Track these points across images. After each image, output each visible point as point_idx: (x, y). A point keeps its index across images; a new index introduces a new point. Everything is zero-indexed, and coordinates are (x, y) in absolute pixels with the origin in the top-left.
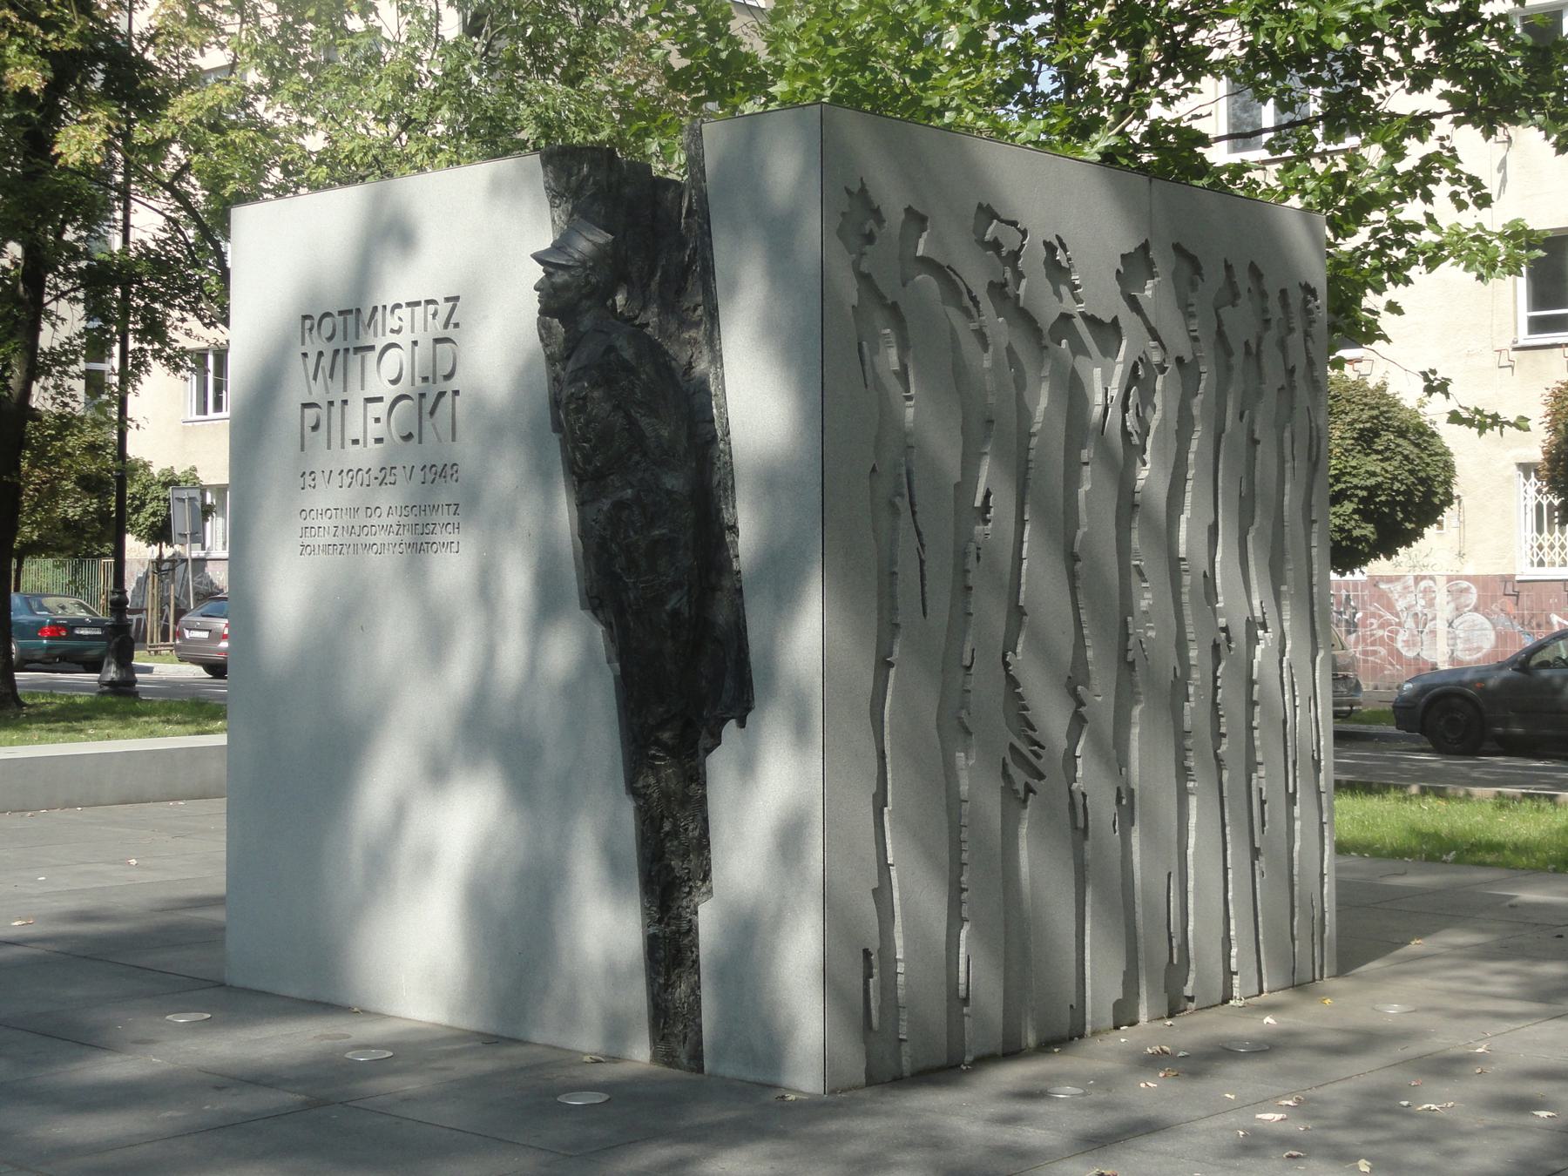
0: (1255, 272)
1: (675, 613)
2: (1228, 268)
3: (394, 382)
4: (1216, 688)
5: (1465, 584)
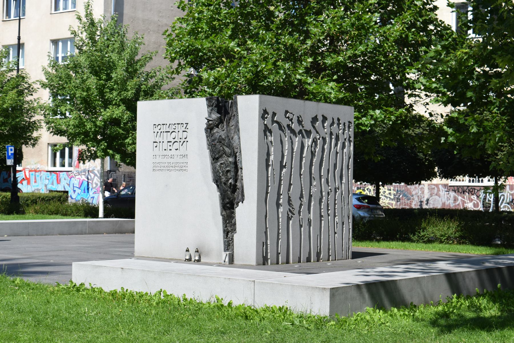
0: (339, 120)
1: (231, 183)
2: (333, 119)
3: (174, 139)
4: (328, 201)
5: (433, 187)
